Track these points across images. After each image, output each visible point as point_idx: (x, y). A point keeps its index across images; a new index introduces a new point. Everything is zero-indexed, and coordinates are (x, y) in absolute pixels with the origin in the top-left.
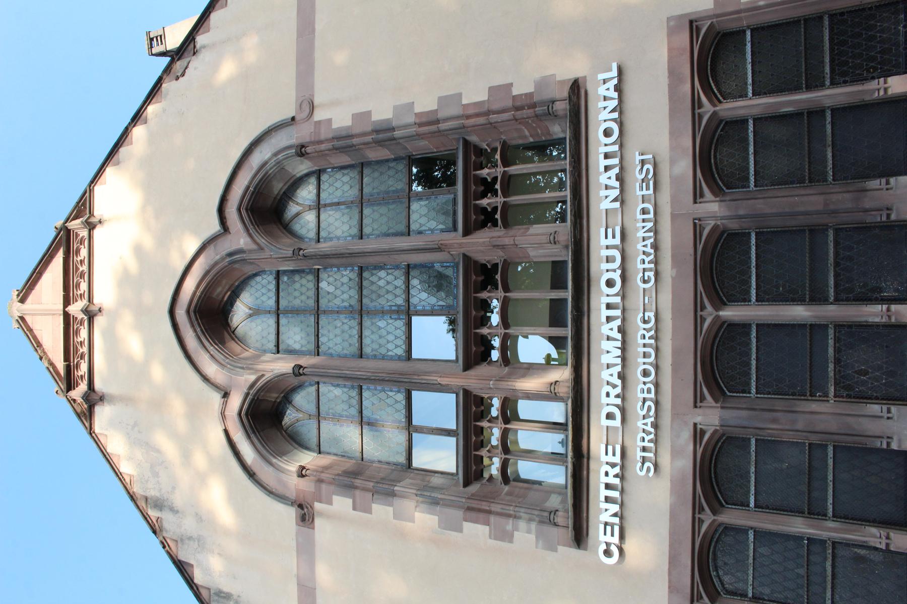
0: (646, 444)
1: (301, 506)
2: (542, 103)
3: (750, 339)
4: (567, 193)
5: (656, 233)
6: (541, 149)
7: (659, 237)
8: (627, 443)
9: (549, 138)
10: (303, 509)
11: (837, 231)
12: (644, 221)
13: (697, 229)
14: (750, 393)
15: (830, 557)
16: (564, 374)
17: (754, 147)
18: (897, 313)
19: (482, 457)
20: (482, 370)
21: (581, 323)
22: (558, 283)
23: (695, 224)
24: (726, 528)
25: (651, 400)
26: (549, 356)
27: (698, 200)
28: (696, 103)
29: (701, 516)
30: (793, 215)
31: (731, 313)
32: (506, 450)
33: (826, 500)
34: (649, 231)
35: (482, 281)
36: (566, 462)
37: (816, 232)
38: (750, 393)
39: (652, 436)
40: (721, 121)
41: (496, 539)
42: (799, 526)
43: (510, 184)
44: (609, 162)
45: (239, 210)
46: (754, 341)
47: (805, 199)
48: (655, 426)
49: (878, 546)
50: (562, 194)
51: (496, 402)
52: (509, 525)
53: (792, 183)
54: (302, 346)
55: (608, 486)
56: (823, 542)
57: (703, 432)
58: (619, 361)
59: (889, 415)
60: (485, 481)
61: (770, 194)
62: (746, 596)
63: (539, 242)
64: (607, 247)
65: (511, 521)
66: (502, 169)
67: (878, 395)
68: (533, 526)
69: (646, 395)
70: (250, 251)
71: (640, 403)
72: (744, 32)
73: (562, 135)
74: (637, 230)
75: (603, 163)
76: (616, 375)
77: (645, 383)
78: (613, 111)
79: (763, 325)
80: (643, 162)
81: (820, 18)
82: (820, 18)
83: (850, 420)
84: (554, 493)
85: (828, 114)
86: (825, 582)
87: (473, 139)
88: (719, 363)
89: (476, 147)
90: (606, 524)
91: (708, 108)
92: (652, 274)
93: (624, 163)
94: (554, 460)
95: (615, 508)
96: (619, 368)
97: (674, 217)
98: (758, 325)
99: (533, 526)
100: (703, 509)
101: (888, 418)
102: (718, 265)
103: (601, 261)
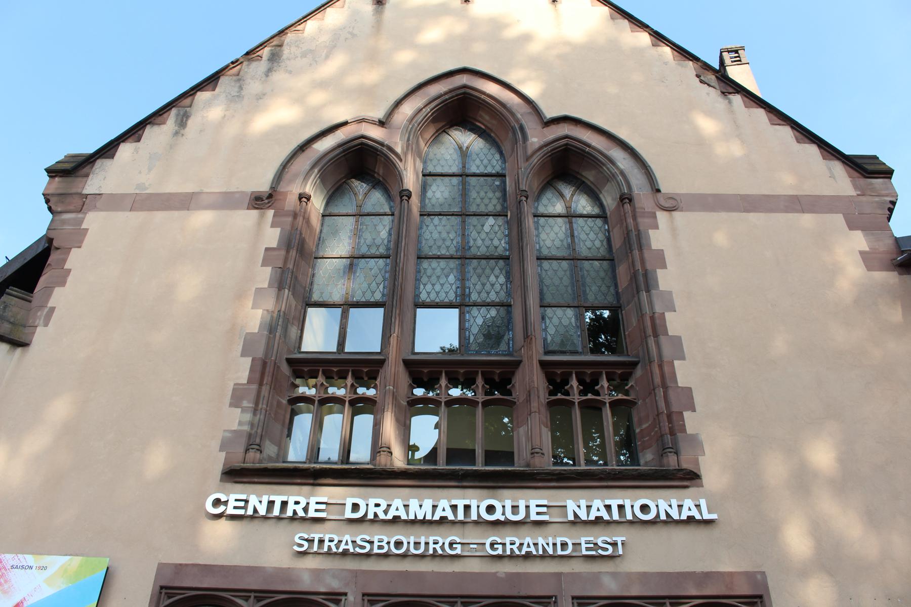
0: (327, 543)
1: (270, 196)
2: (675, 443)
6: (628, 443)
7: (538, 559)
8: (328, 524)
12: (555, 545)
16: (398, 461)
19: (316, 377)
20: (404, 379)
21: (450, 479)
22: (491, 456)
23: (550, 597)
25: (372, 549)
29: (252, 599)
32: (324, 401)
34: (544, 549)
36: (310, 462)
39: (334, 550)
41: (234, 389)
43: (592, 409)
44: (615, 510)
45: (567, 137)
48: (345, 553)
51: (371, 392)
54: (430, 199)
55: (284, 504)
58: (412, 517)
63: (533, 438)
64: (527, 507)
66: (607, 401)
68: (246, 428)
69: (376, 544)
71: (368, 538)
73: (642, 462)
74: (545, 538)
77: (388, 543)
78: (667, 514)
80: (614, 544)
87: (639, 372)
89: (630, 374)
90: (246, 501)
93: (613, 526)
94: (312, 450)
95: (262, 511)
96: (404, 517)
97: (559, 575)
99: (246, 428)
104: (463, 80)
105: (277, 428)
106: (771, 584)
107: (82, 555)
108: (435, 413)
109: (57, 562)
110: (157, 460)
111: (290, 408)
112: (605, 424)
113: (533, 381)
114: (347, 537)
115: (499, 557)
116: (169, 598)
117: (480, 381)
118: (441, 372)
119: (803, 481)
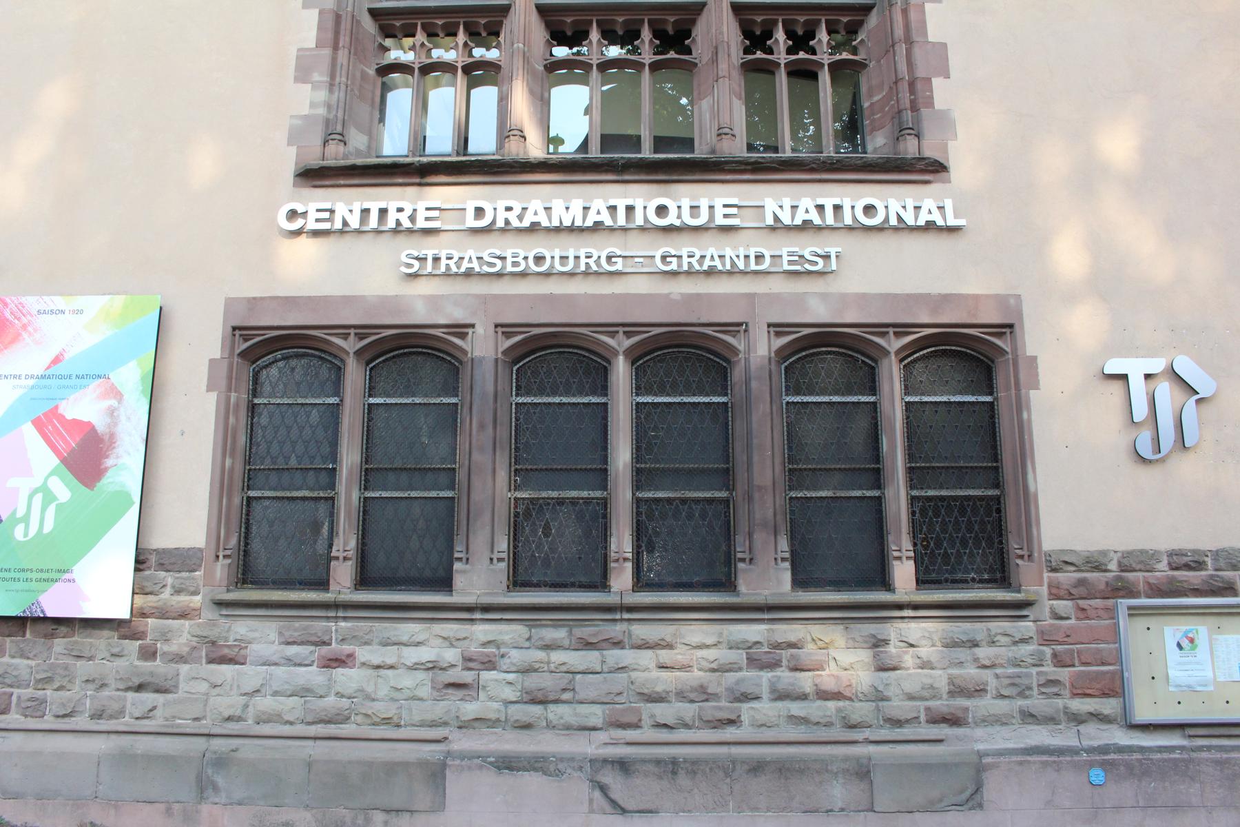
0: (444, 262)
2: (918, 121)
3: (587, 395)
5: (730, 273)
6: (852, 128)
7: (725, 277)
8: (443, 236)
9: (867, 130)
11: (726, 502)
12: (747, 257)
13: (734, 327)
14: (517, 395)
15: (315, 494)
16: (535, 149)
18: (622, 569)
19: (413, 36)
20: (539, 33)
21: (607, 172)
22: (660, 143)
23: (740, 324)
25: (504, 267)
26: (562, 142)
27: (772, 329)
28: (901, 329)
29: (352, 337)
30: (749, 446)
31: (621, 371)
32: (426, 69)
33: (386, 490)
34: (733, 264)
35: (665, 32)
36: (414, 155)
37: (726, 476)
38: (517, 395)
39: (454, 269)
40: (876, 361)
41: (298, 58)
42: (350, 457)
43: (804, 74)
44: (829, 211)
46: (585, 400)
47: (769, 463)
48: (469, 274)
49: (334, 548)
50: (788, 148)
51: (493, 54)
52: (320, 77)
53: (790, 448)
55: (383, 212)
56: (332, 486)
57: (463, 336)
58: (556, 223)
59: (495, 561)
60: (380, 40)
61: (777, 421)
62: (255, 396)
63: (719, 110)
64: (711, 207)
65: (326, 79)
66: (826, 62)
67: (520, 549)
68: (322, 111)
69: (509, 260)
71: (498, 253)
72: (991, 394)
73: (870, 148)
74: (735, 248)
75: (829, 204)
76: (536, 219)
77: (526, 258)
78: (900, 219)
79: (606, 411)
80: (826, 257)
81: (997, 485)
82: (997, 485)
83: (487, 517)
84: (370, 142)
85: (876, 493)
86: (284, 489)
87: (873, 20)
88: (554, 356)
89: (860, 24)
90: (332, 211)
91: (894, 344)
92: (674, 266)
93: (826, 232)
94: (416, 139)
95: (354, 223)
96: (545, 223)
97: (751, 297)
98: (605, 404)
99: (322, 111)
100: (361, 339)
101: (491, 559)
102: (685, 355)
103: (692, 199)
105: (364, 111)
106: (1027, 310)
107: (125, 293)
108: (584, 81)
109: (94, 304)
110: (204, 163)
111: (379, 81)
112: (821, 95)
113: (722, 33)
114: (471, 253)
115: (674, 274)
116: (246, 340)
117: (646, 34)
118: (591, 21)
119: (1089, 177)
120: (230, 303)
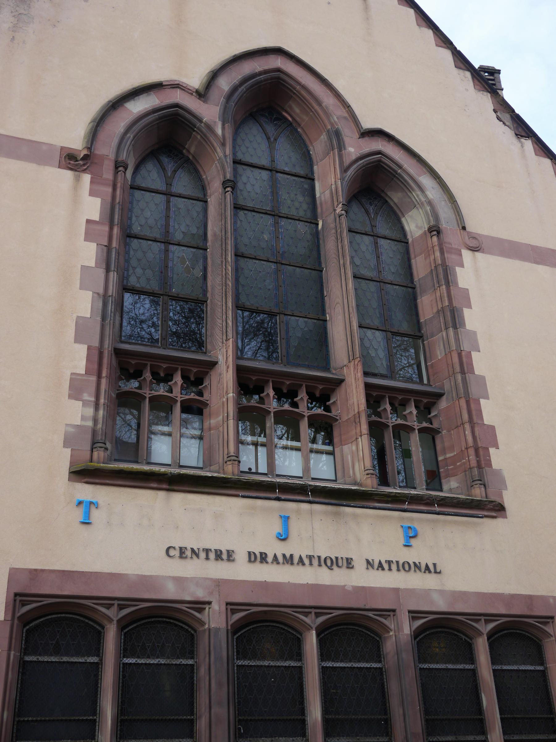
1: (86, 157)
4: (420, 491)
10: (83, 159)
17: (452, 669)
21: (299, 494)
24: (99, 633)
31: (311, 642)
38: (237, 659)
41: (71, 379)
45: (379, 153)
46: (287, 664)
52: (89, 397)
54: (241, 190)
57: (201, 610)
65: (93, 399)
66: (148, 396)
68: (90, 423)
70: (341, 157)
73: (445, 487)
87: (443, 404)
88: (263, 627)
89: (434, 404)
104: (278, 62)
118: (302, 385)
120: (14, 573)
